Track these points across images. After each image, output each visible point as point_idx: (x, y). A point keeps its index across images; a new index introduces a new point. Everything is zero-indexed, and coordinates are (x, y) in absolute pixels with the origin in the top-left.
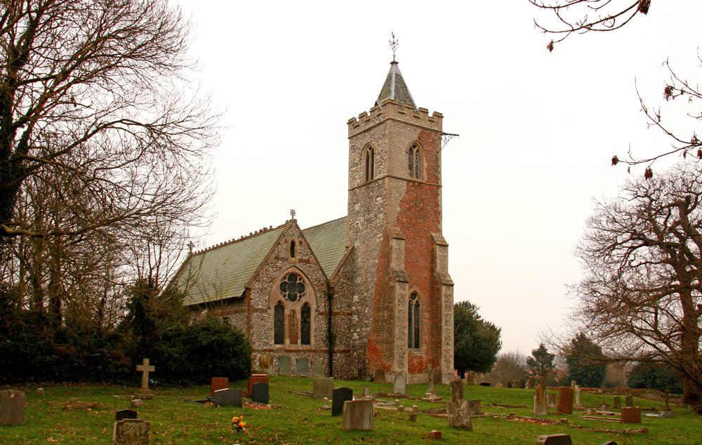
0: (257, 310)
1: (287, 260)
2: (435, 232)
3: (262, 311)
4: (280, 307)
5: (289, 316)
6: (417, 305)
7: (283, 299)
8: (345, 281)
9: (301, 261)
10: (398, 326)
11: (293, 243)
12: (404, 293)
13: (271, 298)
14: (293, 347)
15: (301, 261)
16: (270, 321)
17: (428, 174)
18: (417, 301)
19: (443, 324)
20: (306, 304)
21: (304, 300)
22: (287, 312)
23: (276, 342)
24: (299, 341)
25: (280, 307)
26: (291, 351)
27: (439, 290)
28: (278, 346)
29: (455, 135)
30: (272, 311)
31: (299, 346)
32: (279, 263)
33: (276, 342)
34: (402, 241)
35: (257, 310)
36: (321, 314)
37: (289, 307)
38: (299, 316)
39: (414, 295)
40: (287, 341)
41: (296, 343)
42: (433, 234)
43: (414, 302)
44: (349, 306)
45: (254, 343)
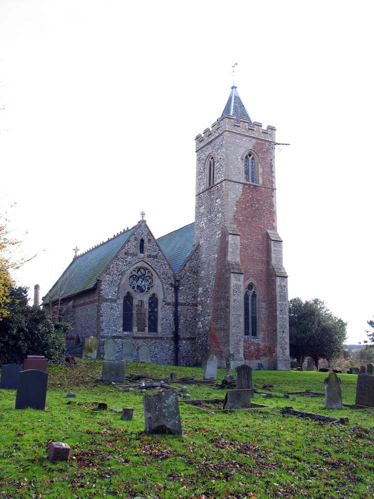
0: (106, 300)
1: (136, 255)
2: (270, 230)
3: (112, 301)
4: (128, 298)
5: (137, 306)
6: (254, 296)
7: (132, 291)
8: (190, 275)
9: (149, 256)
10: (233, 315)
11: (142, 241)
12: (239, 283)
13: (120, 290)
14: (140, 334)
15: (149, 256)
16: (118, 310)
17: (263, 179)
18: (254, 292)
19: (278, 313)
20: (154, 295)
21: (152, 292)
22: (135, 302)
23: (124, 330)
24: (147, 329)
25: (128, 298)
26: (138, 338)
27: (274, 282)
28: (126, 333)
29: (286, 144)
30: (121, 301)
31: (146, 333)
32: (129, 258)
33: (124, 330)
34: (238, 236)
35: (106, 300)
36: (168, 304)
37: (137, 298)
38: (146, 306)
39: (250, 286)
40: (135, 329)
41: (143, 330)
42: (269, 231)
43: (251, 293)
44: (195, 297)
45: (103, 330)
